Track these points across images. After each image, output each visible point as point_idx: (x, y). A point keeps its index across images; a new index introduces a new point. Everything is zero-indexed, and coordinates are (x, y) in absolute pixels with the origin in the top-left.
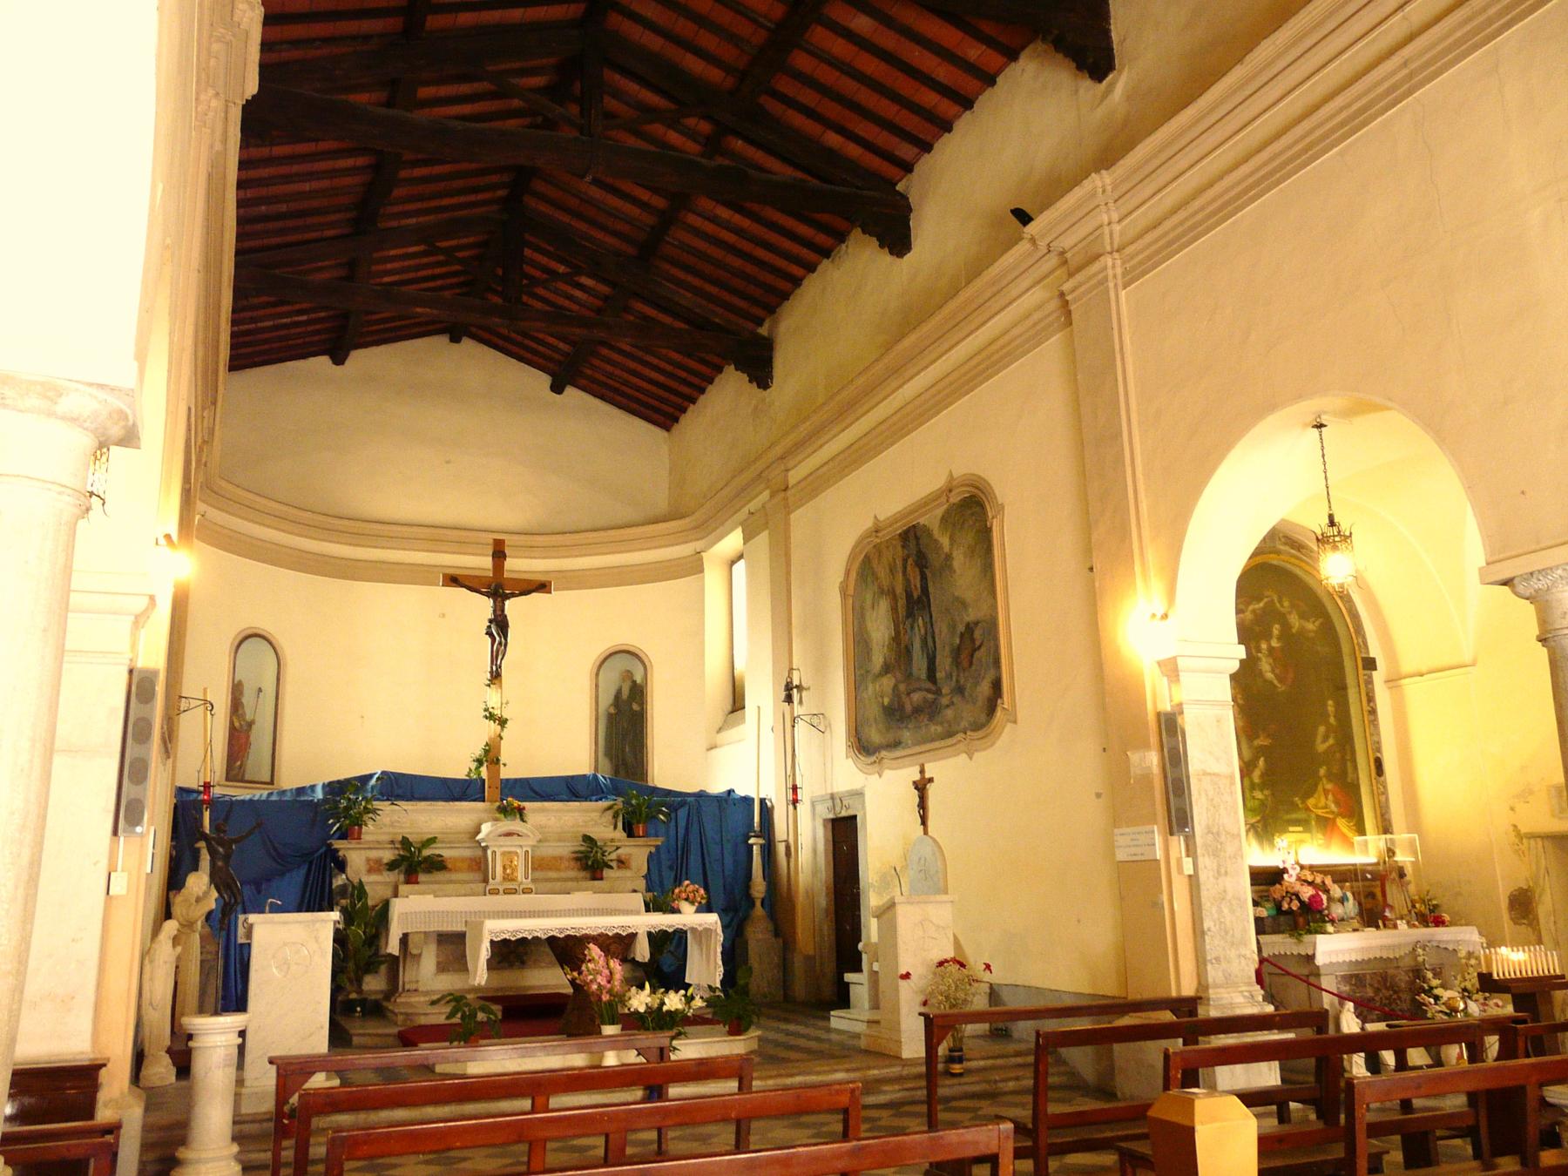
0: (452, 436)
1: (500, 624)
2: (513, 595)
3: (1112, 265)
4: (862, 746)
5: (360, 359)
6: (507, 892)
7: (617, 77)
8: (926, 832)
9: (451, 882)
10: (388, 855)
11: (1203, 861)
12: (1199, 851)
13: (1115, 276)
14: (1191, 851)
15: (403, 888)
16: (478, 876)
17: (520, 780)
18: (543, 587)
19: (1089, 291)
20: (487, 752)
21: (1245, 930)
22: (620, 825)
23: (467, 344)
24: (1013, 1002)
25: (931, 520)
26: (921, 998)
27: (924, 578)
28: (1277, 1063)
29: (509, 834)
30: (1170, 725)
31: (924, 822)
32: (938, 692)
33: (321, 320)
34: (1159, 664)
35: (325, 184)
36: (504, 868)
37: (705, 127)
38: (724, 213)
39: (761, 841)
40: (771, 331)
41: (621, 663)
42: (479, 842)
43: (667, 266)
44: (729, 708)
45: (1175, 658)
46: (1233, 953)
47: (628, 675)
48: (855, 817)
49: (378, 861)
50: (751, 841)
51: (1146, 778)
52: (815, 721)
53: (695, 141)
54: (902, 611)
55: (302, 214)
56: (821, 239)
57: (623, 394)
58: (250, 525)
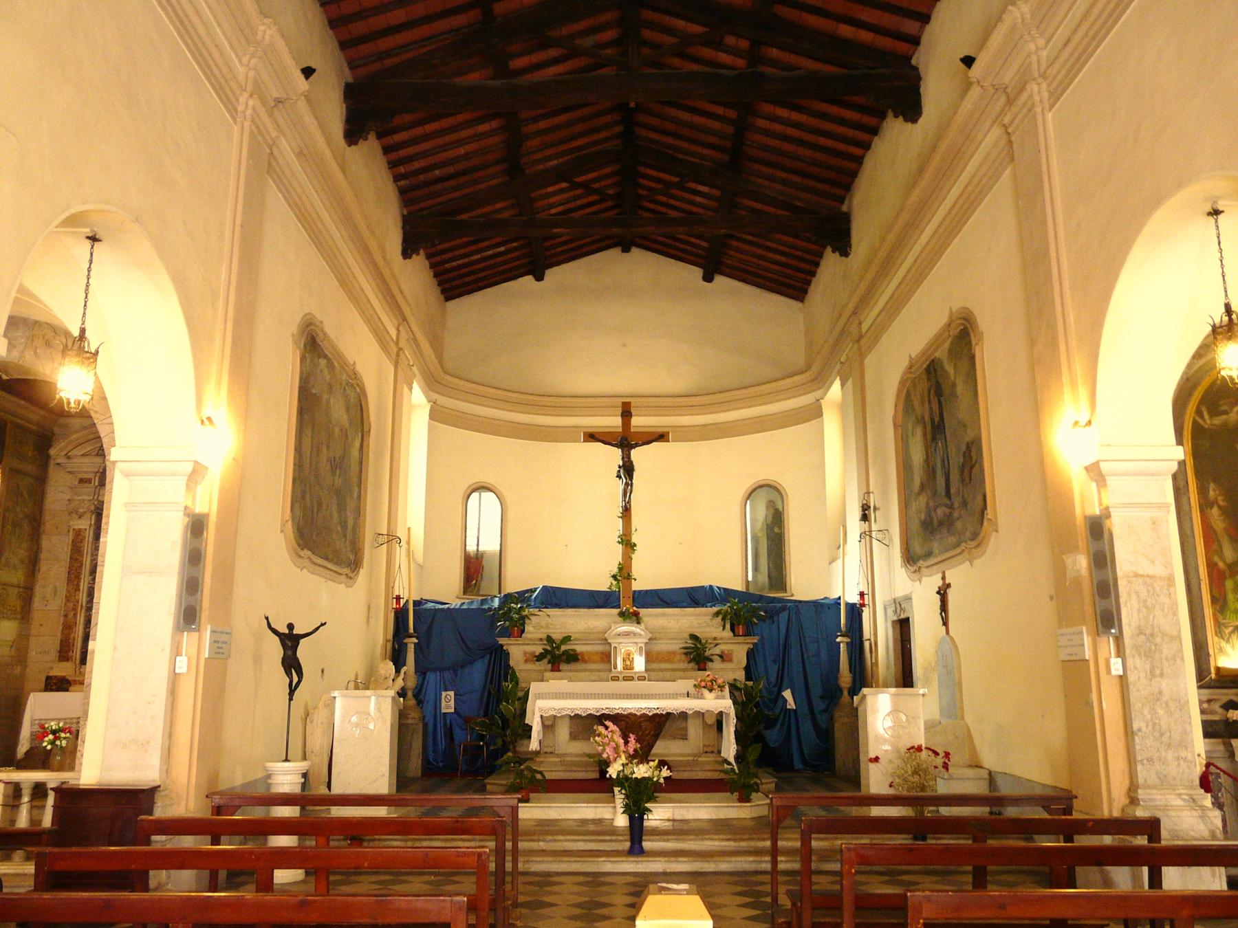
0: (627, 323)
1: (627, 469)
2: (637, 445)
3: (1038, 91)
4: (910, 558)
5: (554, 275)
6: (626, 679)
7: (667, 18)
8: (947, 632)
9: (586, 670)
10: (539, 650)
11: (1135, 662)
12: (1128, 652)
13: (1041, 101)
14: (1120, 653)
15: (548, 674)
18: (662, 437)
19: (1022, 121)
20: (620, 569)
21: (1186, 733)
22: (728, 626)
23: (635, 250)
24: (1005, 789)
25: (941, 354)
26: (888, 784)
27: (940, 402)
28: (1164, 869)
30: (1097, 529)
31: (945, 623)
32: (951, 507)
33: (515, 249)
34: (1086, 469)
35: (474, 146)
37: (744, 44)
38: (782, 112)
39: (847, 640)
40: (850, 207)
43: (757, 166)
45: (1097, 463)
46: (1170, 755)
50: (839, 640)
51: (1077, 581)
53: (742, 58)
54: (929, 437)
55: (465, 172)
56: (867, 120)
57: (764, 278)
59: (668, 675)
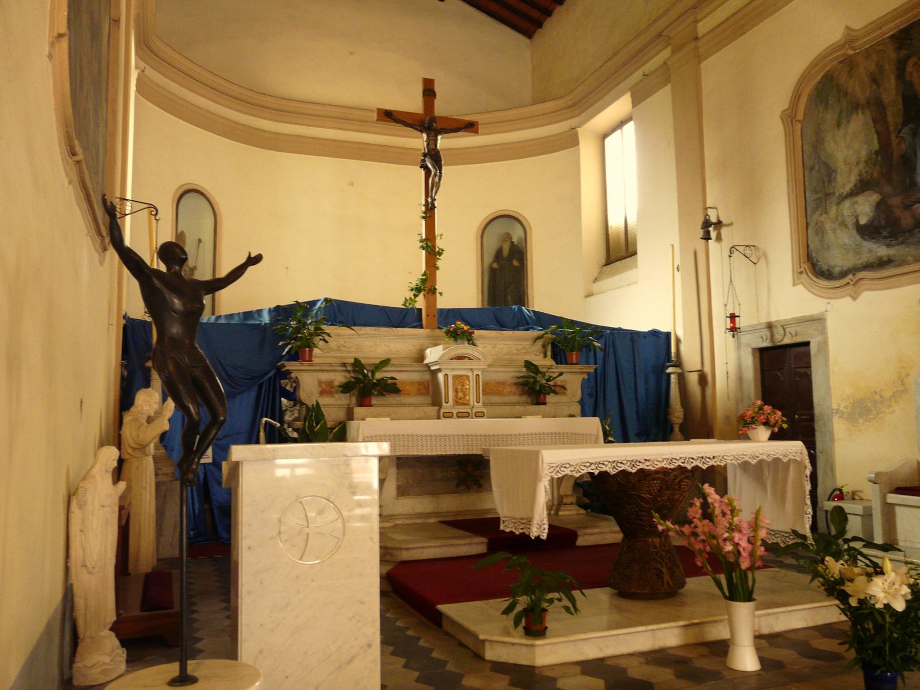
6: (460, 415)
9: (404, 405)
10: (339, 378)
15: (359, 411)
16: (428, 399)
17: (453, 310)
22: (549, 353)
29: (460, 358)
36: (456, 391)
41: (498, 229)
42: (428, 366)
44: (604, 262)
47: (508, 236)
48: (807, 344)
49: (330, 384)
50: (670, 370)
52: (748, 252)
58: (185, 91)
59: (507, 409)
